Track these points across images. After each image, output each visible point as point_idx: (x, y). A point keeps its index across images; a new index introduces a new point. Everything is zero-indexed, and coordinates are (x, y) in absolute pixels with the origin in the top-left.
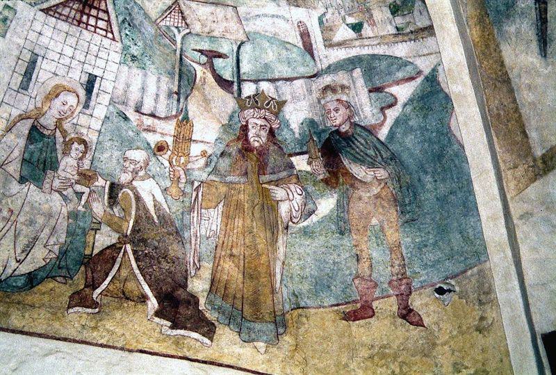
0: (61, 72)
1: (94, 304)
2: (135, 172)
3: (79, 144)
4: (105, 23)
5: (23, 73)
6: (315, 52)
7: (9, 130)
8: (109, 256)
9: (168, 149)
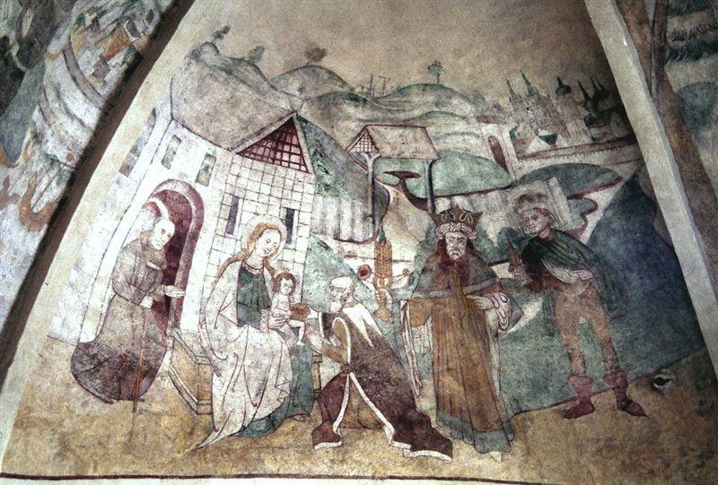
0: (262, 210)
1: (336, 438)
2: (344, 300)
3: (287, 279)
4: (298, 157)
5: (227, 217)
6: (508, 164)
7: (220, 275)
8: (337, 384)
9: (371, 272)
